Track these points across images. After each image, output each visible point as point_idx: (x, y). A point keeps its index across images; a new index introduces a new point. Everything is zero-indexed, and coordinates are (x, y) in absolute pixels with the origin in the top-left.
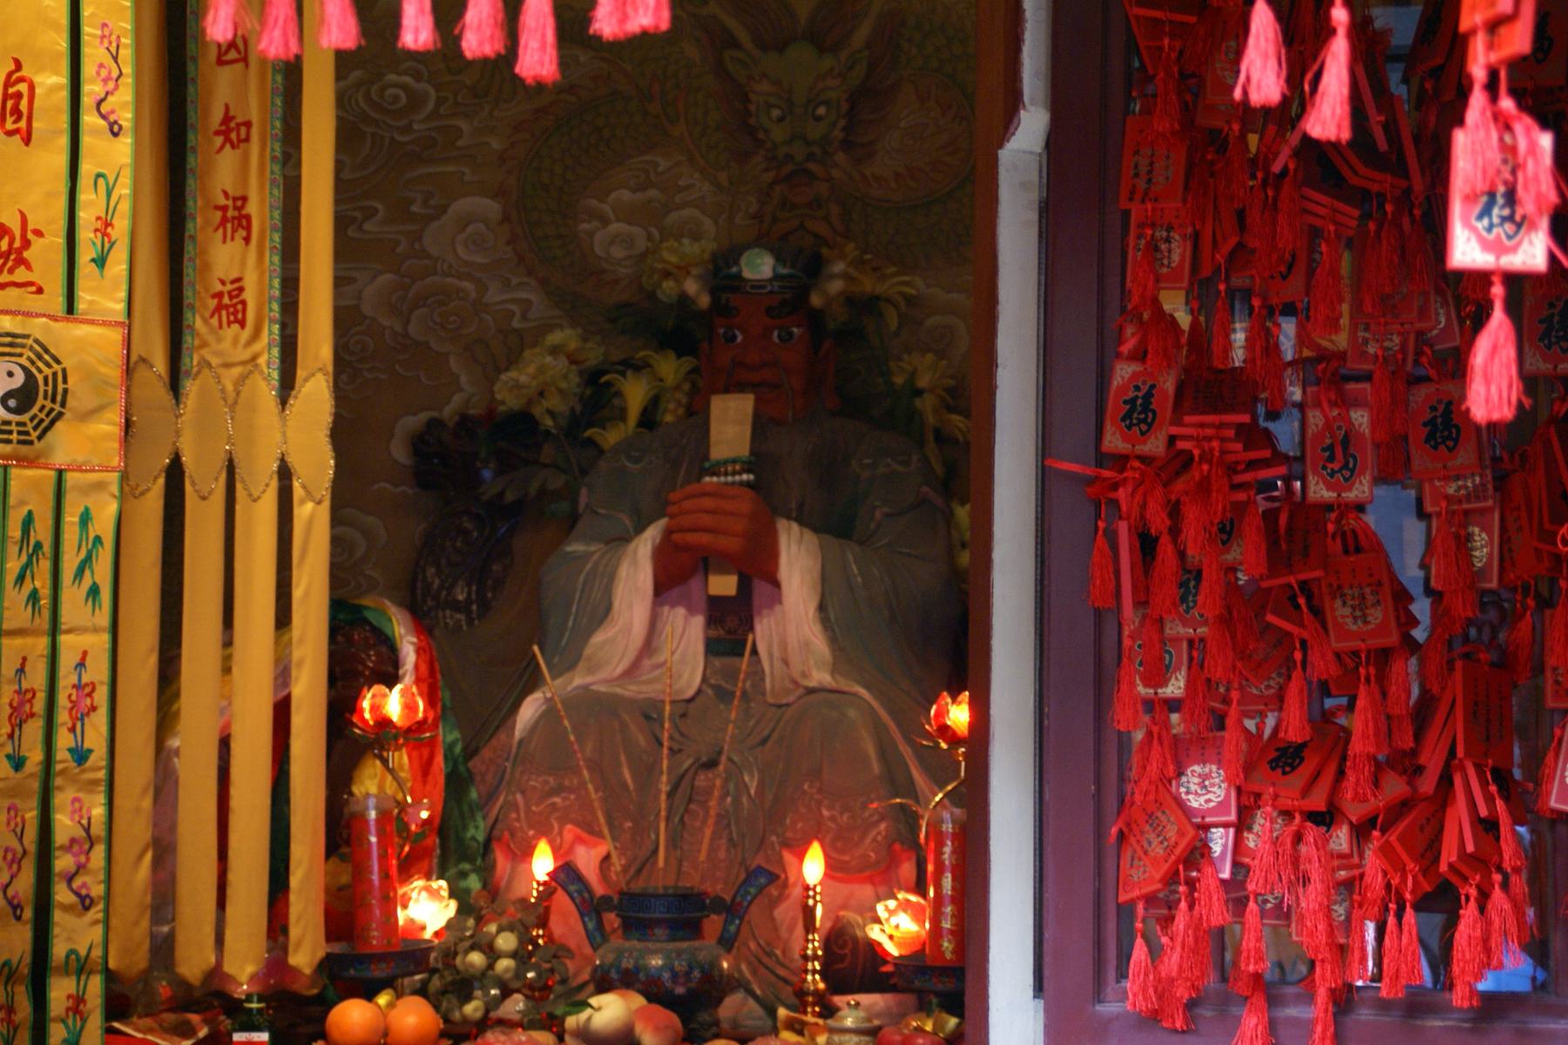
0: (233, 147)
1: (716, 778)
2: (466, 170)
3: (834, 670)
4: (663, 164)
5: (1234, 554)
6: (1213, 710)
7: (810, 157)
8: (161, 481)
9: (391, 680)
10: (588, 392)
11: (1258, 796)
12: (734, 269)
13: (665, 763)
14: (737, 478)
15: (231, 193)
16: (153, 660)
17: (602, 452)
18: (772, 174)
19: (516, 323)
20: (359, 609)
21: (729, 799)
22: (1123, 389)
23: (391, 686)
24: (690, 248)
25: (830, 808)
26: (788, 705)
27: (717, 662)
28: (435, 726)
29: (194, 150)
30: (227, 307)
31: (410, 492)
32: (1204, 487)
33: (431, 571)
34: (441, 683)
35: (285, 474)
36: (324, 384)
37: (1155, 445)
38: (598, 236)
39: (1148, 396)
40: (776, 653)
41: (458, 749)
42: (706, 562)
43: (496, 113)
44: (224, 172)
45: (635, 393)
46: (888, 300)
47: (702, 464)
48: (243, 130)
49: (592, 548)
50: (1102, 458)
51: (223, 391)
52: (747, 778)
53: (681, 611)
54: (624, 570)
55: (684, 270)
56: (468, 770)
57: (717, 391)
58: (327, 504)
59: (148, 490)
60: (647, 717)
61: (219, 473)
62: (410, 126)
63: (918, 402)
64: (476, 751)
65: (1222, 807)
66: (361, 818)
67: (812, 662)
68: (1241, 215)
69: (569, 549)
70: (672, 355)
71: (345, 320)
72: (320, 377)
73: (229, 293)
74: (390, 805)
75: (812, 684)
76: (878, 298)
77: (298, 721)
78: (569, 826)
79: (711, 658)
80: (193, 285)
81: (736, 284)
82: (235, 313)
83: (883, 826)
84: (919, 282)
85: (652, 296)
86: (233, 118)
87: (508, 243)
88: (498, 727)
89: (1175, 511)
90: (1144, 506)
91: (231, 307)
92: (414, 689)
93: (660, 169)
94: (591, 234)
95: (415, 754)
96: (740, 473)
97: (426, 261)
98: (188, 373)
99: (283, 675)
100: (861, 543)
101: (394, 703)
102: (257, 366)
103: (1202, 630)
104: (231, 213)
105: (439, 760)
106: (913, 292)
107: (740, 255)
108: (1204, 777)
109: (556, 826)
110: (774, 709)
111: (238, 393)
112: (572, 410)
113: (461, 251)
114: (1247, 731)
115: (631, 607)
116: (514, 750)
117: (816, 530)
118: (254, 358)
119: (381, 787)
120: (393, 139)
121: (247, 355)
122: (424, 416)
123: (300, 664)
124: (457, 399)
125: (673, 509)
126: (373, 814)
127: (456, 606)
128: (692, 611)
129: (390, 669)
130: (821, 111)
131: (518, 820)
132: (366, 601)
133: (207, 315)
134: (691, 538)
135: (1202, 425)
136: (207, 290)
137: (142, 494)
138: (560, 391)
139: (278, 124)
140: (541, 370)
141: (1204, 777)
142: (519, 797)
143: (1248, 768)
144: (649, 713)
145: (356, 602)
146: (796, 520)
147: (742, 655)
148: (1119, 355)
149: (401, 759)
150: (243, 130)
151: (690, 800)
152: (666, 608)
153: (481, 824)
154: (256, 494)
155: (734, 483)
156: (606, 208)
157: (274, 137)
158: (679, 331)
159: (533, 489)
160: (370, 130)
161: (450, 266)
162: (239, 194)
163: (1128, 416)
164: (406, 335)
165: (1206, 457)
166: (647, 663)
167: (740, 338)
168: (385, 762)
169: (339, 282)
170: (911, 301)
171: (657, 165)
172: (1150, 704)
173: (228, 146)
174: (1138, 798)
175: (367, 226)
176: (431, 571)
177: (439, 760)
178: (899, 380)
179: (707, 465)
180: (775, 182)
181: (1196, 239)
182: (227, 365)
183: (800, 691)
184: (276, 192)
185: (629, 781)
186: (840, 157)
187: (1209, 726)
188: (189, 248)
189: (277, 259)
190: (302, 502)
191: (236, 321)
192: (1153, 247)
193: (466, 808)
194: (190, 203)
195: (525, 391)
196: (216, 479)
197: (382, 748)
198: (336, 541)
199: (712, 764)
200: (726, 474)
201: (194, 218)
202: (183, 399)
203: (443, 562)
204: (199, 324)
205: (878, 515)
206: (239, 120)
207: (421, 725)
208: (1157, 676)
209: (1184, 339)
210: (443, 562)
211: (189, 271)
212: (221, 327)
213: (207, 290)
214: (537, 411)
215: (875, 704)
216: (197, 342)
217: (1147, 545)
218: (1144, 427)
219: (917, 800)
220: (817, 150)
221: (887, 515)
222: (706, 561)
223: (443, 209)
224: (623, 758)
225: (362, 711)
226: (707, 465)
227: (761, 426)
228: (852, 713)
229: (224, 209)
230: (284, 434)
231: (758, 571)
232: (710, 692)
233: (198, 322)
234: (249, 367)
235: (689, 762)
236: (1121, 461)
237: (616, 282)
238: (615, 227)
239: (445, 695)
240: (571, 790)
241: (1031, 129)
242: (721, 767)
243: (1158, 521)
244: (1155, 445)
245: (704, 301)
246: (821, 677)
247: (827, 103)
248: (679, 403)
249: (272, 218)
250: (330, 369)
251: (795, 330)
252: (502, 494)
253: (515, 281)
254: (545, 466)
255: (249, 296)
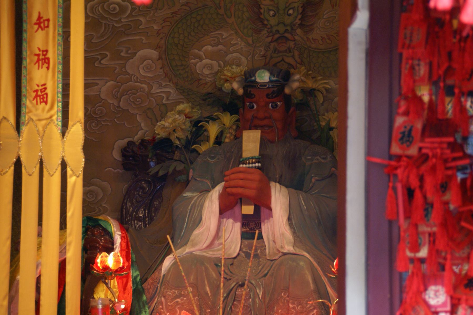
0: (42, 29)
1: (242, 292)
2: (143, 38)
3: (294, 245)
4: (225, 35)
5: (447, 197)
6: (439, 264)
7: (286, 31)
8: (12, 168)
9: (109, 250)
10: (194, 129)
11: (459, 300)
12: (253, 78)
13: (222, 284)
14: (254, 165)
15: (41, 49)
16: (9, 243)
17: (199, 154)
18: (270, 39)
19: (164, 102)
20: (97, 220)
21: (251, 300)
22: (399, 128)
23: (109, 253)
24: (235, 69)
25: (293, 303)
26: (275, 260)
27: (246, 242)
28: (128, 268)
29: (26, 31)
30: (40, 96)
31: (121, 171)
32: (433, 169)
33: (129, 204)
34: (131, 251)
35: (64, 165)
36: (80, 127)
37: (413, 151)
38: (198, 65)
39: (410, 131)
40: (271, 238)
41: (138, 279)
42: (241, 200)
43: (155, 15)
44: (38, 40)
45: (213, 130)
46: (318, 90)
47: (240, 160)
48: (46, 23)
49: (194, 195)
50: (391, 157)
51: (38, 130)
52: (258, 291)
53: (231, 221)
54: (207, 204)
55: (233, 78)
56: (142, 287)
57: (246, 129)
58: (81, 177)
59: (7, 172)
60: (217, 265)
61: (37, 164)
62: (120, 20)
63: (331, 133)
64: (146, 280)
65: (444, 304)
66: (96, 308)
67: (285, 242)
68: (450, 55)
69: (185, 195)
70: (229, 114)
71: (88, 100)
72: (78, 124)
73: (41, 90)
74: (107, 303)
75: (285, 251)
76: (314, 89)
77: (69, 267)
78: (183, 311)
79: (243, 240)
80: (25, 87)
81: (254, 84)
82: (43, 98)
83: (315, 311)
84: (332, 83)
85: (220, 89)
86: (42, 18)
87: (161, 69)
88: (155, 269)
89: (421, 179)
90: (408, 177)
91: (41, 95)
92: (119, 254)
93: (224, 37)
94: (195, 64)
95: (120, 281)
96: (255, 163)
97: (127, 76)
98: (23, 123)
99: (63, 250)
100: (306, 192)
101: (110, 260)
102: (52, 120)
103: (435, 229)
104: (41, 57)
105: (130, 284)
106: (329, 87)
107: (256, 72)
108: (436, 291)
109: (178, 311)
110: (270, 262)
111: (44, 131)
112: (187, 137)
113: (141, 71)
114: (455, 273)
115: (210, 219)
116: (161, 279)
117: (287, 187)
118: (51, 117)
119: (106, 295)
120: (113, 25)
121: (48, 115)
122: (126, 140)
123: (70, 244)
124: (140, 133)
125: (226, 178)
126: (100, 307)
127: (139, 219)
128: (235, 220)
129: (110, 246)
130: (291, 12)
131: (162, 308)
132: (101, 217)
133: (32, 99)
134: (234, 190)
135: (433, 143)
136: (31, 89)
137: (4, 174)
138: (182, 129)
139: (61, 20)
140: (174, 121)
141: (436, 291)
142: (163, 299)
143: (455, 288)
144: (216, 263)
145: (97, 218)
146: (279, 183)
147: (254, 239)
148: (398, 114)
149: (114, 283)
150: (46, 23)
151: (234, 300)
152: (225, 220)
153: (147, 310)
154: (52, 173)
155: (252, 167)
156: (201, 53)
157: (59, 25)
158: (232, 104)
159: (171, 170)
160: (104, 22)
161: (137, 78)
162: (45, 49)
163: (402, 139)
164: (119, 107)
165: (435, 156)
166: (217, 242)
167: (255, 107)
168: (107, 284)
169: (87, 86)
170: (327, 90)
171: (222, 35)
172: (412, 260)
173: (40, 29)
174: (408, 300)
175: (103, 62)
176: (129, 204)
177: (130, 284)
178: (323, 124)
179: (241, 160)
180: (272, 41)
181: (431, 65)
182: (40, 120)
183: (281, 254)
184: (60, 48)
185: (209, 292)
186: (299, 31)
187: (436, 270)
188: (24, 72)
189: (60, 76)
190: (71, 176)
191: (44, 102)
192: (412, 68)
193: (141, 304)
194: (24, 53)
195: (167, 129)
196: (35, 167)
197: (105, 279)
198: (85, 194)
199: (242, 285)
200: (249, 164)
201: (26, 59)
202: (21, 134)
203: (134, 201)
204: (28, 103)
205: (313, 180)
206: (45, 18)
207: (121, 269)
208: (416, 248)
209: (426, 106)
210: (134, 201)
211: (24, 81)
212: (37, 104)
213: (31, 89)
214: (173, 138)
215: (312, 260)
216: (27, 111)
217: (410, 193)
218: (408, 143)
219: (330, 301)
220: (289, 28)
221: (317, 180)
222: (241, 199)
223: (135, 54)
224: (206, 282)
225: (97, 263)
226: (241, 160)
227: (263, 144)
228: (302, 263)
229: (38, 55)
230: (64, 148)
231: (262, 204)
232: (243, 254)
233: (28, 102)
234: (49, 121)
235: (234, 284)
236: (399, 158)
237: (206, 84)
238: (205, 61)
239: (133, 256)
240: (184, 296)
241: (362, 20)
242: (245, 286)
243: (414, 183)
244: (413, 151)
245: (241, 92)
246: (289, 248)
247: (293, 8)
248: (231, 134)
249: (58, 59)
250: (83, 121)
251: (278, 103)
252: (157, 172)
253: (164, 84)
254: (176, 160)
255: (49, 91)
